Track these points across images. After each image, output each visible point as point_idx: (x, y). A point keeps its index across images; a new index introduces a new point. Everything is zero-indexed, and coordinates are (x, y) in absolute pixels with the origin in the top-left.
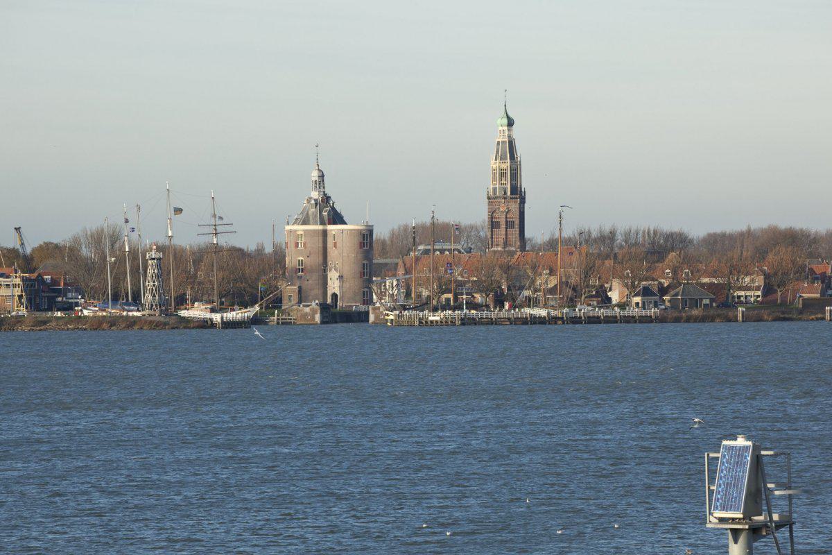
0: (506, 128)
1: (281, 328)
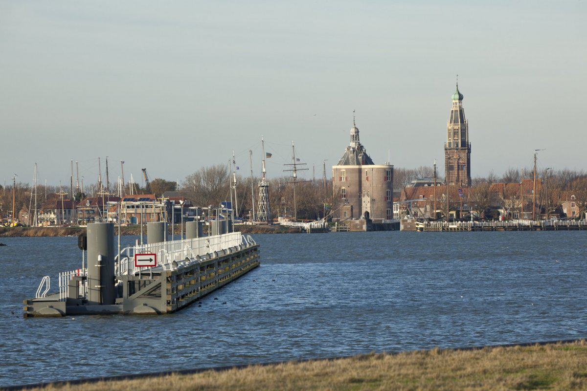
0: (458, 101)
1: (340, 233)
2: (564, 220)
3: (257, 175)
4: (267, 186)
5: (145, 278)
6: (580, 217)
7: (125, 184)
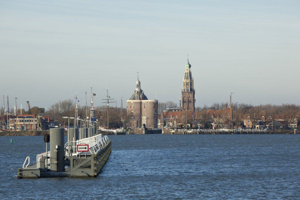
0: (188, 68)
2: (245, 129)
3: (89, 105)
4: (94, 111)
5: (82, 158)
6: (252, 127)
7: (17, 109)
